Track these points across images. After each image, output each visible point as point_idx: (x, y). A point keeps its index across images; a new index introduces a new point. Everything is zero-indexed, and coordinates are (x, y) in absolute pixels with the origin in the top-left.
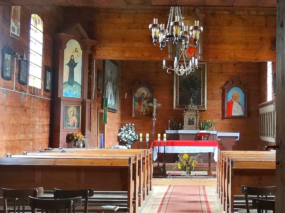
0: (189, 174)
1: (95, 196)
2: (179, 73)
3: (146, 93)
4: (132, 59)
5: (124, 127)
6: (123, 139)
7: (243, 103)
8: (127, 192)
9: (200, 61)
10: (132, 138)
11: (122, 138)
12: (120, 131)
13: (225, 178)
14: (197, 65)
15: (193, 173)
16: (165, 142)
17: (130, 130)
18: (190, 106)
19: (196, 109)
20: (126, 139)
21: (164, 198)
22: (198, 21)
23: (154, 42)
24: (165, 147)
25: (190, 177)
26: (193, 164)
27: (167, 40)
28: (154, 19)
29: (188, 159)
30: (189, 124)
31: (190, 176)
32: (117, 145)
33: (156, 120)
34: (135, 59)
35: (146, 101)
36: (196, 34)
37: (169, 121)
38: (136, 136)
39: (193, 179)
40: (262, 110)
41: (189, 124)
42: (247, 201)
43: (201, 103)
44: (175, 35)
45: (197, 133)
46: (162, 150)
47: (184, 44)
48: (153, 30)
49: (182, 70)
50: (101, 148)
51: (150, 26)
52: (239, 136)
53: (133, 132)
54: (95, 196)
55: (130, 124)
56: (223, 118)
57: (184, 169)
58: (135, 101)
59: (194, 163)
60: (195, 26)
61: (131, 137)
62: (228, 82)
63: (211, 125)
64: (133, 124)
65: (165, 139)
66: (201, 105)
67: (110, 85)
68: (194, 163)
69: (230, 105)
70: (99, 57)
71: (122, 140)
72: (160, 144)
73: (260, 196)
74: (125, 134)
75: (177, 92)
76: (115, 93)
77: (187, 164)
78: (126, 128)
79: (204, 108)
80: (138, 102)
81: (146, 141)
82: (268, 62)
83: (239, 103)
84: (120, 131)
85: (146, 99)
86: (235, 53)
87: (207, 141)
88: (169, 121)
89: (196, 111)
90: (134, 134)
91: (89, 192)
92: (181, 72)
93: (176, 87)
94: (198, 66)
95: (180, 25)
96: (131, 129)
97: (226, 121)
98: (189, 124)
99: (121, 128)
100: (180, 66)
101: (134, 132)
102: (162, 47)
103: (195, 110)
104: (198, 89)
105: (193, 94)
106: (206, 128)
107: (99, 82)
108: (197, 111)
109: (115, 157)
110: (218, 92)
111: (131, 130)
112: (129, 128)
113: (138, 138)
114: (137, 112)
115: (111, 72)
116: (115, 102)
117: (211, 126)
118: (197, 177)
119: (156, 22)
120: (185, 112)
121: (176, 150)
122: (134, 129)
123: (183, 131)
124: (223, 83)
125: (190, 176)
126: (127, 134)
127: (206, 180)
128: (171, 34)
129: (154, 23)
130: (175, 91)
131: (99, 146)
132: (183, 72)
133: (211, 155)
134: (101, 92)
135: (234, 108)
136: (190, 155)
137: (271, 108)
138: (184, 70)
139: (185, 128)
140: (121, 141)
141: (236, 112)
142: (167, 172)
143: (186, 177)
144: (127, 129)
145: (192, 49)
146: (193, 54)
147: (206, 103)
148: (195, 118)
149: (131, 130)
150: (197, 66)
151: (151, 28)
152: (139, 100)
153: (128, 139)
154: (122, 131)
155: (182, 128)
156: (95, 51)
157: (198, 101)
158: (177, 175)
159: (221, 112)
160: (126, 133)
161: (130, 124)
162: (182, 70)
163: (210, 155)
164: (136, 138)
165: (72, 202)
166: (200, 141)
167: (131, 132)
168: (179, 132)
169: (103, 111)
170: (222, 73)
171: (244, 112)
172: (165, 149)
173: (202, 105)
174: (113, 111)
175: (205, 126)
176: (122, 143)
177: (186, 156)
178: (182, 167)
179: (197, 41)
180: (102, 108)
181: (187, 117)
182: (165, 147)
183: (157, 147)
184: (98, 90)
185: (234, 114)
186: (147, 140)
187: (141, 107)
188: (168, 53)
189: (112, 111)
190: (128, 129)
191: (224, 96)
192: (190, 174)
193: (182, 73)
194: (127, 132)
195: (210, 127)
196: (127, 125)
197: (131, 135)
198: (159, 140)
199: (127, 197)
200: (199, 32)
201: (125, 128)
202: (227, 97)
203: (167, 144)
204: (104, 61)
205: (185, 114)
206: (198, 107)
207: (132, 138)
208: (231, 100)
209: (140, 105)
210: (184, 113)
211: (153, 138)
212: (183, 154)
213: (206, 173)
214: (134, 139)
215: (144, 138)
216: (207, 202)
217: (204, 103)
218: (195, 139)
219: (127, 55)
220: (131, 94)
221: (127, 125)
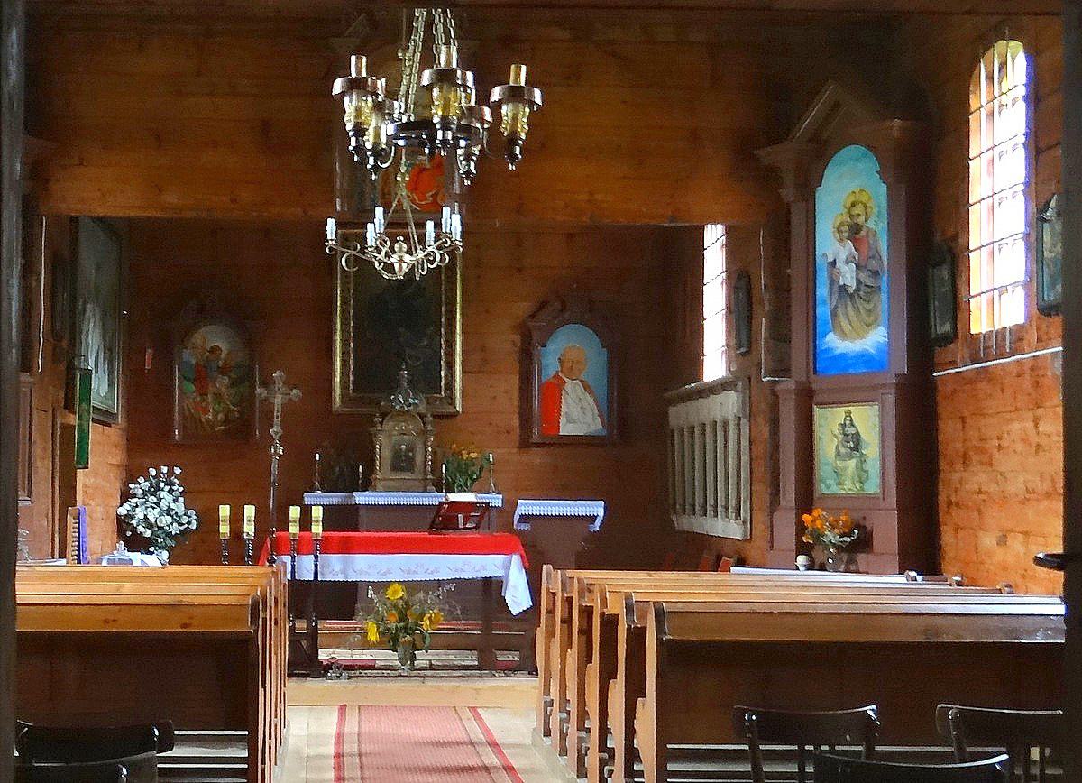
0: (409, 662)
1: (177, 752)
2: (389, 267)
3: (224, 347)
4: (193, 214)
5: (141, 479)
6: (140, 529)
7: (600, 383)
8: (246, 733)
9: (397, 223)
10: (172, 524)
11: (134, 522)
12: (126, 496)
13: (608, 674)
14: (458, 238)
15: (422, 658)
16: (317, 540)
17: (163, 494)
18: (400, 398)
19: (422, 408)
20: (150, 526)
21: (338, 756)
22: (524, 68)
23: (355, 148)
24: (316, 557)
25: (415, 673)
26: (426, 623)
27: (401, 143)
28: (513, 66)
29: (407, 603)
30: (395, 468)
31: (413, 668)
32: (122, 553)
33: (281, 453)
34: (205, 215)
35: (226, 380)
36: (515, 118)
37: (318, 458)
38: (189, 517)
39: (429, 682)
40: (679, 415)
41: (395, 468)
42: (802, 768)
43: (441, 387)
44: (439, 120)
45: (441, 504)
46: (306, 568)
47: (462, 158)
48: (350, 104)
49: (401, 261)
50: (79, 562)
51: (338, 85)
52: (601, 512)
53: (176, 500)
54: (177, 752)
55: (165, 469)
56: (525, 444)
57: (391, 642)
58: (184, 378)
59: (430, 618)
60: (511, 84)
61: (169, 519)
62: (542, 305)
63: (478, 473)
64: (178, 471)
65: (317, 529)
66: (438, 395)
67: (94, 315)
68: (430, 618)
69: (553, 391)
70: (63, 206)
71: (134, 529)
72: (298, 548)
73: (807, 747)
74: (147, 508)
75: (345, 342)
76: (109, 350)
77: (402, 624)
78: (147, 484)
79: (453, 404)
80: (195, 381)
81: (245, 535)
82: (709, 226)
83: (587, 388)
84: (126, 496)
85: (223, 371)
86: (591, 194)
87: (475, 535)
88: (318, 458)
89: (422, 416)
90: (179, 508)
91: (157, 733)
92: (397, 266)
93: (345, 324)
94: (461, 244)
95: (459, 82)
96: (167, 488)
97: (537, 457)
98: (395, 468)
99: (131, 486)
100: (394, 242)
101: (181, 499)
102: (376, 167)
103: (419, 415)
104: (429, 332)
105: (408, 351)
106: (461, 486)
107: (59, 307)
108: (426, 419)
109: (181, 598)
110: (504, 342)
111: (168, 492)
112: (162, 485)
113: (194, 522)
114: (191, 424)
115: (98, 268)
116: (111, 385)
117: (481, 474)
118: (441, 673)
119: (359, 70)
120: (381, 423)
121: (358, 568)
122: (181, 489)
123: (372, 493)
124: (522, 308)
125: (413, 668)
126: (154, 508)
127: (463, 684)
128: (412, 119)
129: (354, 75)
130: (338, 338)
131: (73, 553)
132: (404, 265)
133: (494, 586)
134: (65, 344)
135: (566, 402)
136: (411, 586)
137: (728, 405)
138: (407, 258)
139: (379, 487)
140: (129, 534)
141: (574, 421)
142: (323, 655)
143: (396, 673)
144: (154, 490)
145: (425, 175)
146: (431, 194)
147: (458, 385)
148: (419, 446)
149: (168, 492)
150: (457, 242)
151: (343, 94)
152: (200, 376)
153: (156, 529)
154: (135, 496)
155: (367, 486)
156: (48, 181)
157: (429, 380)
158: (363, 666)
159: (516, 422)
160: (148, 504)
161: (165, 469)
162: (401, 261)
163: (491, 588)
164: (189, 523)
165: (124, 770)
166: (451, 535)
167: (170, 498)
168: (357, 499)
169: (73, 420)
170: (519, 270)
171: (607, 422)
172: (316, 566)
173: (442, 393)
174: (105, 418)
175: (455, 475)
176: (137, 543)
177: (396, 594)
178: (381, 634)
179: (518, 144)
180: (69, 406)
181: (386, 441)
182: (316, 557)
183: (287, 559)
184: (54, 335)
185: (566, 429)
186: (249, 529)
187: (204, 400)
188: (332, 191)
189: (102, 418)
190: (158, 489)
191: (527, 358)
192: (412, 663)
193: (401, 270)
194: (153, 499)
195: (474, 480)
196: (153, 472)
197: (168, 512)
198: (294, 529)
199: (245, 754)
200: (527, 110)
201: (145, 485)
202: (540, 364)
203: (327, 547)
204: (74, 221)
205: (379, 428)
206: (428, 403)
207: (172, 524)
208: (556, 376)
209: (203, 394)
210: (374, 425)
211: (273, 520)
212: (385, 585)
213: (471, 659)
214: (182, 528)
215: (237, 519)
216: (509, 769)
217: (450, 387)
218: (431, 527)
219: (171, 198)
220: (167, 352)
221: (153, 472)
